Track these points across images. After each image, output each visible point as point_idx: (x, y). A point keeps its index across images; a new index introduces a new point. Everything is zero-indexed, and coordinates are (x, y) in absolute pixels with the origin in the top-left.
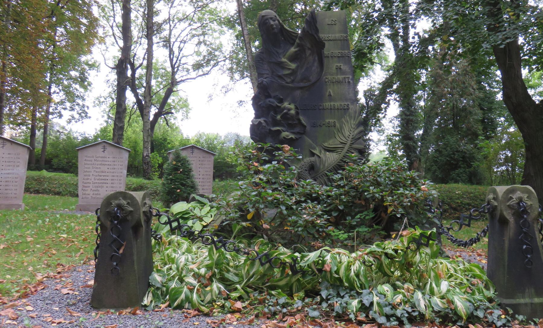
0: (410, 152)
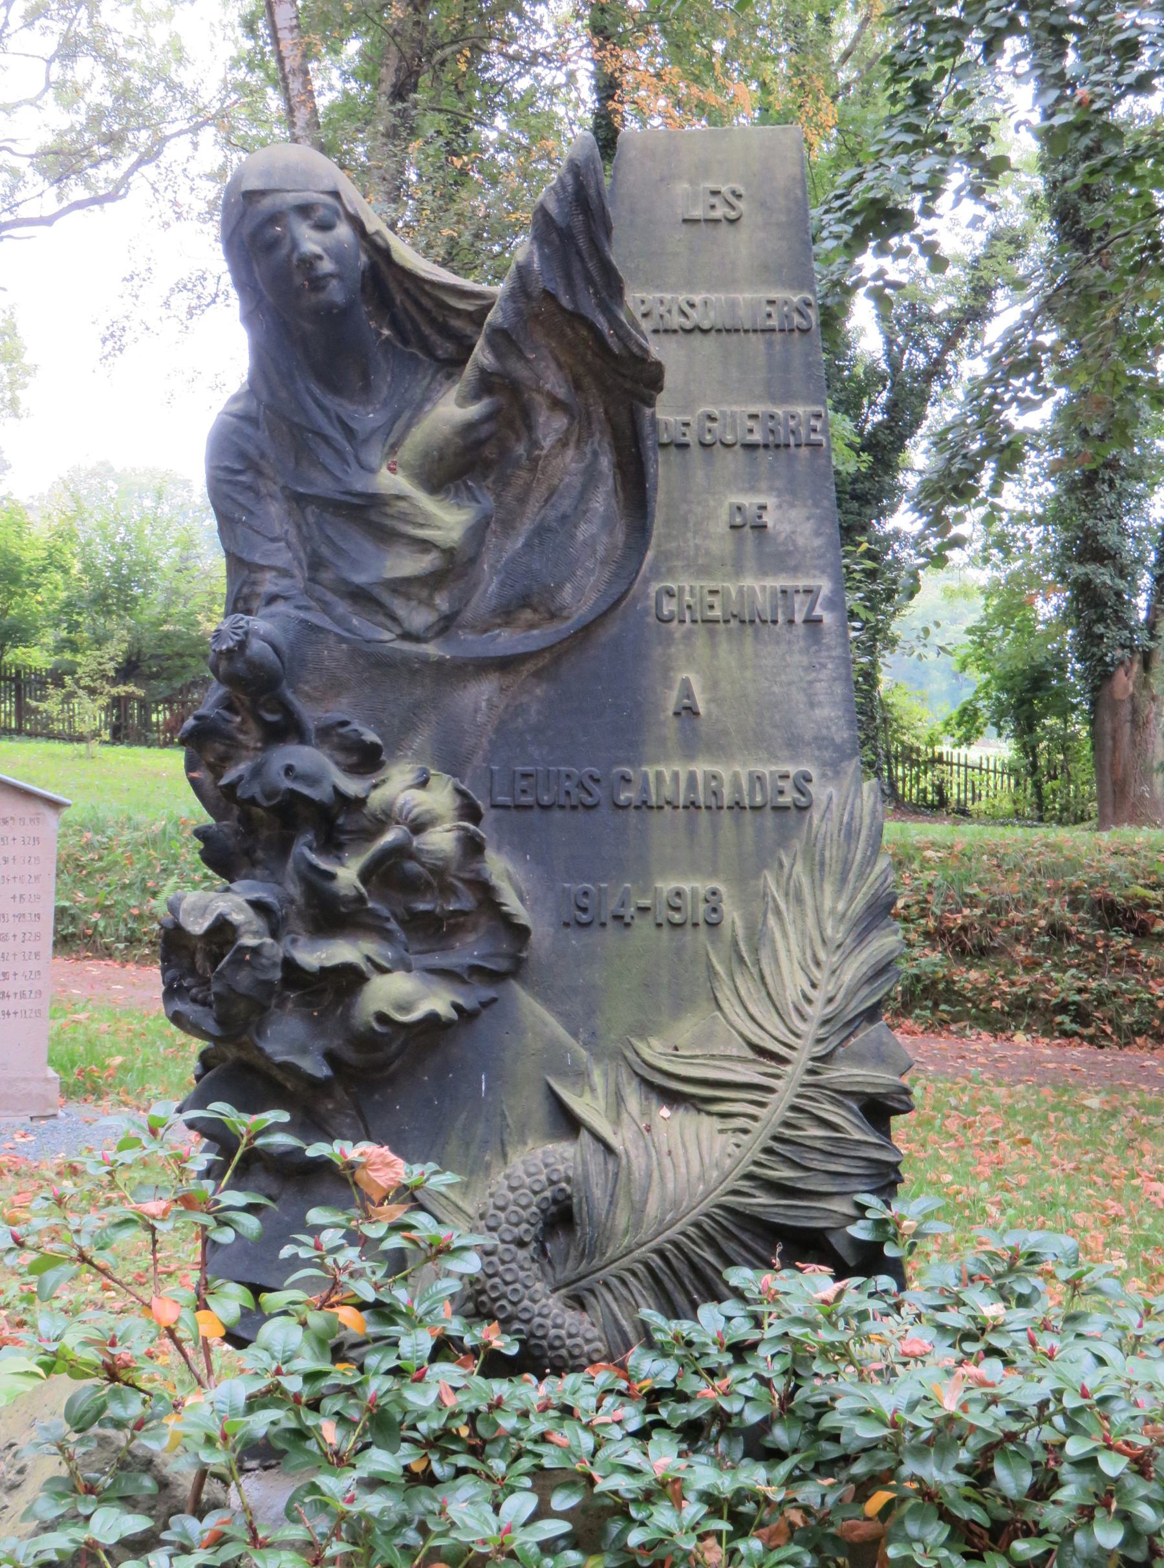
0: (1102, 619)
